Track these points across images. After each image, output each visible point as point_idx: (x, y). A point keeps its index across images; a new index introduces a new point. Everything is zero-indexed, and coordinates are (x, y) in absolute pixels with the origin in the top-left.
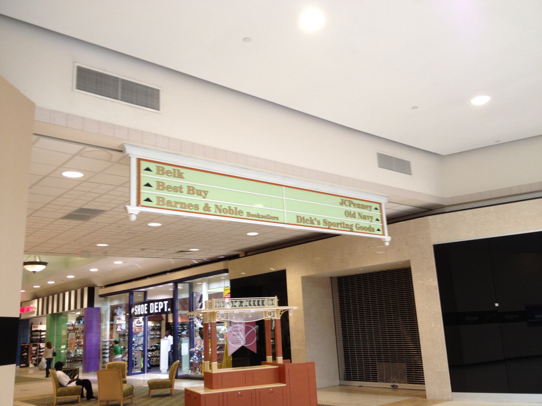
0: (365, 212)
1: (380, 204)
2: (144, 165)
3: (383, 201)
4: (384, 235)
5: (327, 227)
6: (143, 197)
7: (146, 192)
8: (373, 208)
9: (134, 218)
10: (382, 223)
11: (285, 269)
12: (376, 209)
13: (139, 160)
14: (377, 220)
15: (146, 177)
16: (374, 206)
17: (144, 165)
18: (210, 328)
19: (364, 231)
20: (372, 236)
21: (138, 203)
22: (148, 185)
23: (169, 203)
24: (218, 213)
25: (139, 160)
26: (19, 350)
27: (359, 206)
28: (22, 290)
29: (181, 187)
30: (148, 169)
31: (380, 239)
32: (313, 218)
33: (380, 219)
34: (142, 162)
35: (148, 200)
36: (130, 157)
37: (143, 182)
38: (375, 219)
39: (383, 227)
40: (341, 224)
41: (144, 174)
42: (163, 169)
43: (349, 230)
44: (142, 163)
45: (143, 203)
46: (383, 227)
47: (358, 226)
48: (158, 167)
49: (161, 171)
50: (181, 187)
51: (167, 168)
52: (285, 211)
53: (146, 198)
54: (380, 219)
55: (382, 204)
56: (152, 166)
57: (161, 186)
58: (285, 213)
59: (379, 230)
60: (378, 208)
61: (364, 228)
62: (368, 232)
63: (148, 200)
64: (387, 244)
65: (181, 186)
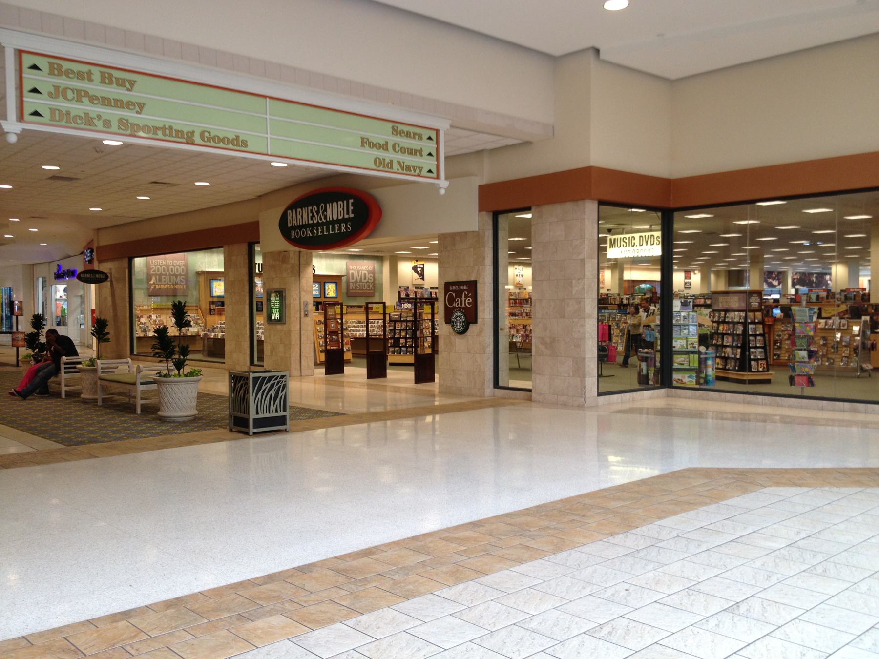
0: (414, 144)
1: (437, 131)
2: (28, 60)
3: (443, 126)
4: (438, 177)
5: (129, 132)
6: (28, 110)
7: (31, 102)
8: (425, 137)
9: (13, 139)
10: (438, 159)
11: (254, 219)
12: (430, 138)
13: (20, 53)
14: (430, 154)
15: (31, 79)
16: (426, 134)
17: (28, 60)
18: (696, 278)
19: (221, 145)
20: (37, 129)
21: (21, 118)
22: (35, 90)
23: (408, 168)
24: (400, 171)
25: (20, 53)
26: (53, 300)
27: (408, 135)
28: (510, 251)
29: (421, 151)
30: (35, 67)
31: (433, 184)
32: (92, 115)
33: (434, 153)
34: (24, 56)
35: (36, 113)
36: (4, 47)
37: (27, 87)
38: (425, 153)
39: (438, 166)
40: (163, 129)
41: (28, 74)
42: (60, 67)
43: (184, 140)
44: (25, 56)
45: (27, 117)
46: (438, 166)
47: (206, 134)
48: (102, 74)
49: (56, 70)
50: (421, 151)
51: (66, 65)
52: (269, 136)
53: (32, 111)
54: (434, 153)
55: (6, 49)
56: (39, 62)
57: (58, 92)
58: (269, 139)
59: (430, 171)
60: (434, 137)
61: (222, 140)
62: (230, 146)
63: (36, 113)
64: (443, 192)
65: (421, 149)
